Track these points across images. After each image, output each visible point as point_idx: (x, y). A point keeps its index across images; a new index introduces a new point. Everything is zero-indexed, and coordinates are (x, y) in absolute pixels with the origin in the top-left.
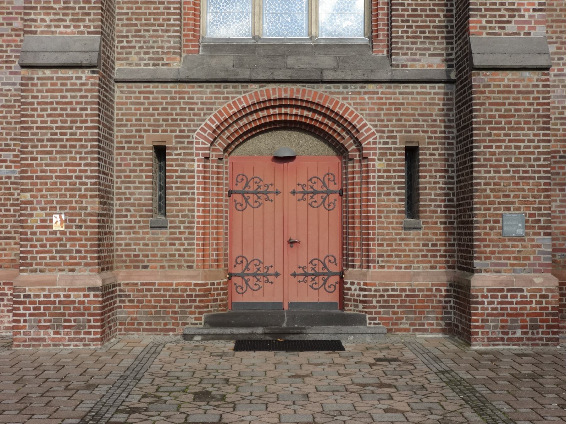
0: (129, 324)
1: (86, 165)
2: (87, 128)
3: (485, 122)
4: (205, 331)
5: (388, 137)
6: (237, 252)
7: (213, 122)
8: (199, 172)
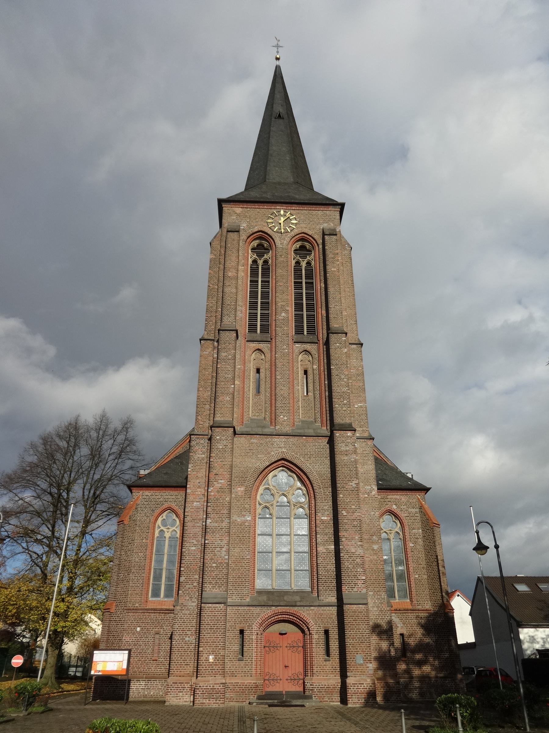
0: (230, 699)
1: (221, 638)
2: (222, 624)
3: (348, 623)
4: (258, 701)
5: (318, 626)
6: (267, 671)
7: (260, 621)
8: (255, 639)
